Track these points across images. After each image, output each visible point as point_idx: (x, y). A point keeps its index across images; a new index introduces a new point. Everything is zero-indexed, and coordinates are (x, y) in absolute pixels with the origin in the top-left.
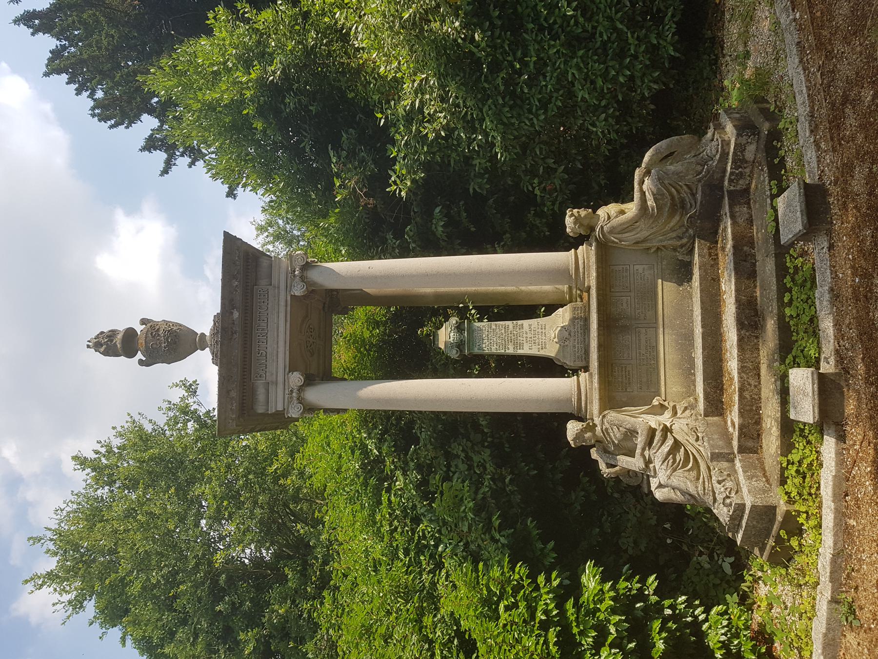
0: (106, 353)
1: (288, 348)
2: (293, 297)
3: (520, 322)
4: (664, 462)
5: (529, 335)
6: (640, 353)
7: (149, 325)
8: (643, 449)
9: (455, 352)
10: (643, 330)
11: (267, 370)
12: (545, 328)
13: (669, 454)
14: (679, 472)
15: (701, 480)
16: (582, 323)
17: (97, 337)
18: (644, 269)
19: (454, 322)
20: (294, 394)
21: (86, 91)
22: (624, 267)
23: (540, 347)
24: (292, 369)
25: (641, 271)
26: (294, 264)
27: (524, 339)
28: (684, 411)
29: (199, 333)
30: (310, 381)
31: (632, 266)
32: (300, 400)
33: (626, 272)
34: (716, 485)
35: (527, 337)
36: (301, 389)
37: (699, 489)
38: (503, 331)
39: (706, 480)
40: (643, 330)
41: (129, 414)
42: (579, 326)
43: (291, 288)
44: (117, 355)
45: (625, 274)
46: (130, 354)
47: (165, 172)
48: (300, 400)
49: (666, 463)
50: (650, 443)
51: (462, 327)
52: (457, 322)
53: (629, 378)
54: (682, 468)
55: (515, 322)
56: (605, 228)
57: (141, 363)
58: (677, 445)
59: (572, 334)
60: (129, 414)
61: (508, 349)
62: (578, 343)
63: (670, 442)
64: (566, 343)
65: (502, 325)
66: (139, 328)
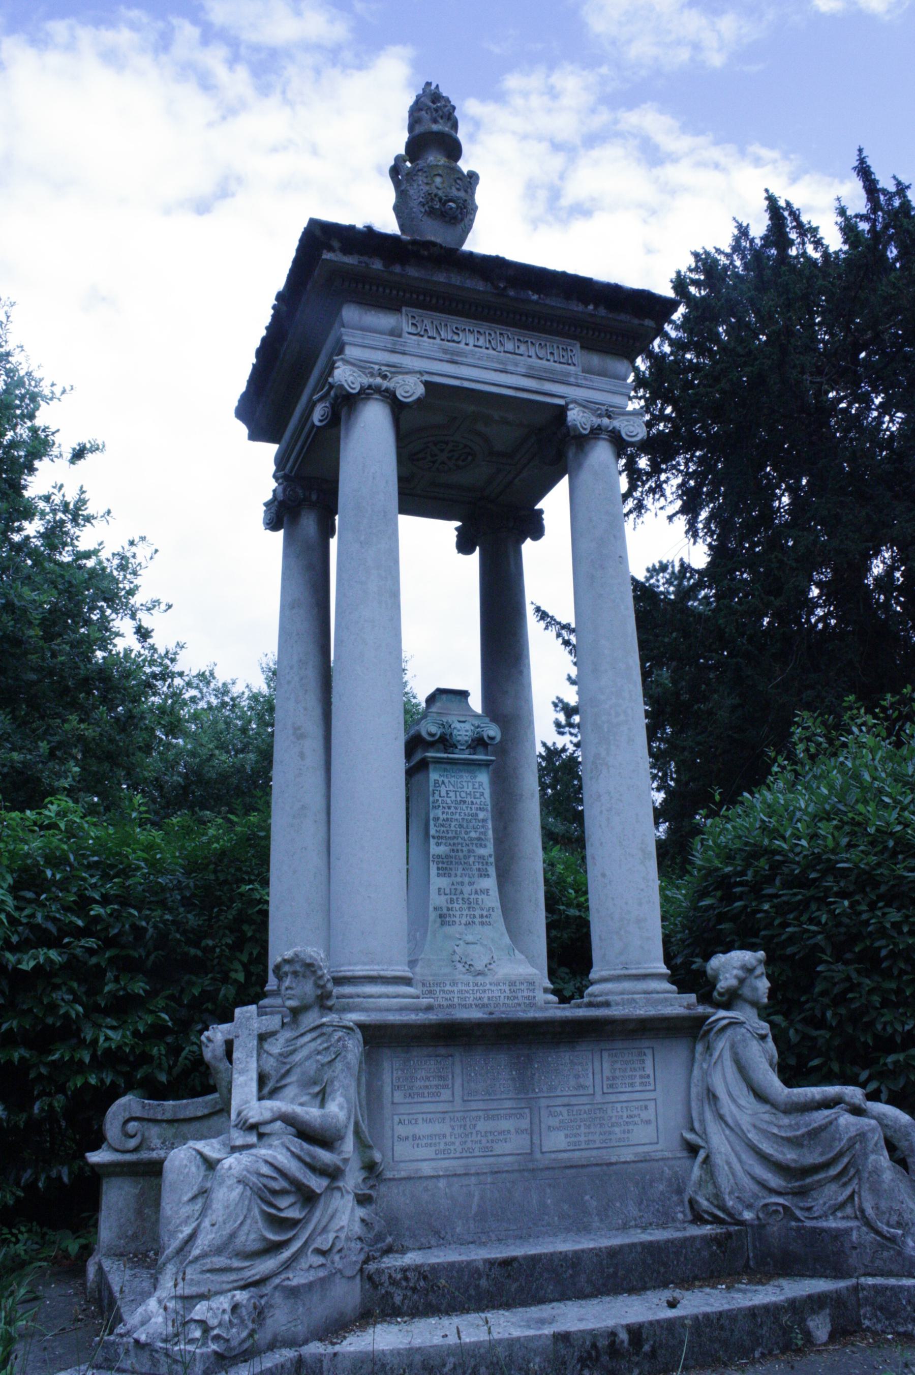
1: (466, 384)
3: (492, 871)
5: (467, 889)
6: (478, 1118)
8: (288, 1120)
9: (433, 729)
10: (525, 1124)
11: (425, 339)
12: (482, 924)
15: (236, 1263)
16: (502, 1001)
19: (492, 733)
20: (379, 380)
21: (765, 238)
22: (651, 1080)
23: (445, 911)
24: (427, 384)
25: (644, 1115)
26: (622, 418)
27: (459, 879)
31: (652, 1095)
33: (641, 1084)
35: (462, 883)
37: (215, 1259)
38: (473, 835)
39: (233, 1277)
40: (525, 1124)
41: (58, 431)
42: (497, 994)
44: (411, 128)
45: (638, 1080)
51: (480, 749)
52: (492, 738)
53: (423, 1095)
54: (263, 1212)
55: (492, 860)
59: (480, 979)
60: (58, 431)
61: (438, 844)
62: (460, 992)
63: (317, 1184)
64: (459, 966)
65: (485, 833)
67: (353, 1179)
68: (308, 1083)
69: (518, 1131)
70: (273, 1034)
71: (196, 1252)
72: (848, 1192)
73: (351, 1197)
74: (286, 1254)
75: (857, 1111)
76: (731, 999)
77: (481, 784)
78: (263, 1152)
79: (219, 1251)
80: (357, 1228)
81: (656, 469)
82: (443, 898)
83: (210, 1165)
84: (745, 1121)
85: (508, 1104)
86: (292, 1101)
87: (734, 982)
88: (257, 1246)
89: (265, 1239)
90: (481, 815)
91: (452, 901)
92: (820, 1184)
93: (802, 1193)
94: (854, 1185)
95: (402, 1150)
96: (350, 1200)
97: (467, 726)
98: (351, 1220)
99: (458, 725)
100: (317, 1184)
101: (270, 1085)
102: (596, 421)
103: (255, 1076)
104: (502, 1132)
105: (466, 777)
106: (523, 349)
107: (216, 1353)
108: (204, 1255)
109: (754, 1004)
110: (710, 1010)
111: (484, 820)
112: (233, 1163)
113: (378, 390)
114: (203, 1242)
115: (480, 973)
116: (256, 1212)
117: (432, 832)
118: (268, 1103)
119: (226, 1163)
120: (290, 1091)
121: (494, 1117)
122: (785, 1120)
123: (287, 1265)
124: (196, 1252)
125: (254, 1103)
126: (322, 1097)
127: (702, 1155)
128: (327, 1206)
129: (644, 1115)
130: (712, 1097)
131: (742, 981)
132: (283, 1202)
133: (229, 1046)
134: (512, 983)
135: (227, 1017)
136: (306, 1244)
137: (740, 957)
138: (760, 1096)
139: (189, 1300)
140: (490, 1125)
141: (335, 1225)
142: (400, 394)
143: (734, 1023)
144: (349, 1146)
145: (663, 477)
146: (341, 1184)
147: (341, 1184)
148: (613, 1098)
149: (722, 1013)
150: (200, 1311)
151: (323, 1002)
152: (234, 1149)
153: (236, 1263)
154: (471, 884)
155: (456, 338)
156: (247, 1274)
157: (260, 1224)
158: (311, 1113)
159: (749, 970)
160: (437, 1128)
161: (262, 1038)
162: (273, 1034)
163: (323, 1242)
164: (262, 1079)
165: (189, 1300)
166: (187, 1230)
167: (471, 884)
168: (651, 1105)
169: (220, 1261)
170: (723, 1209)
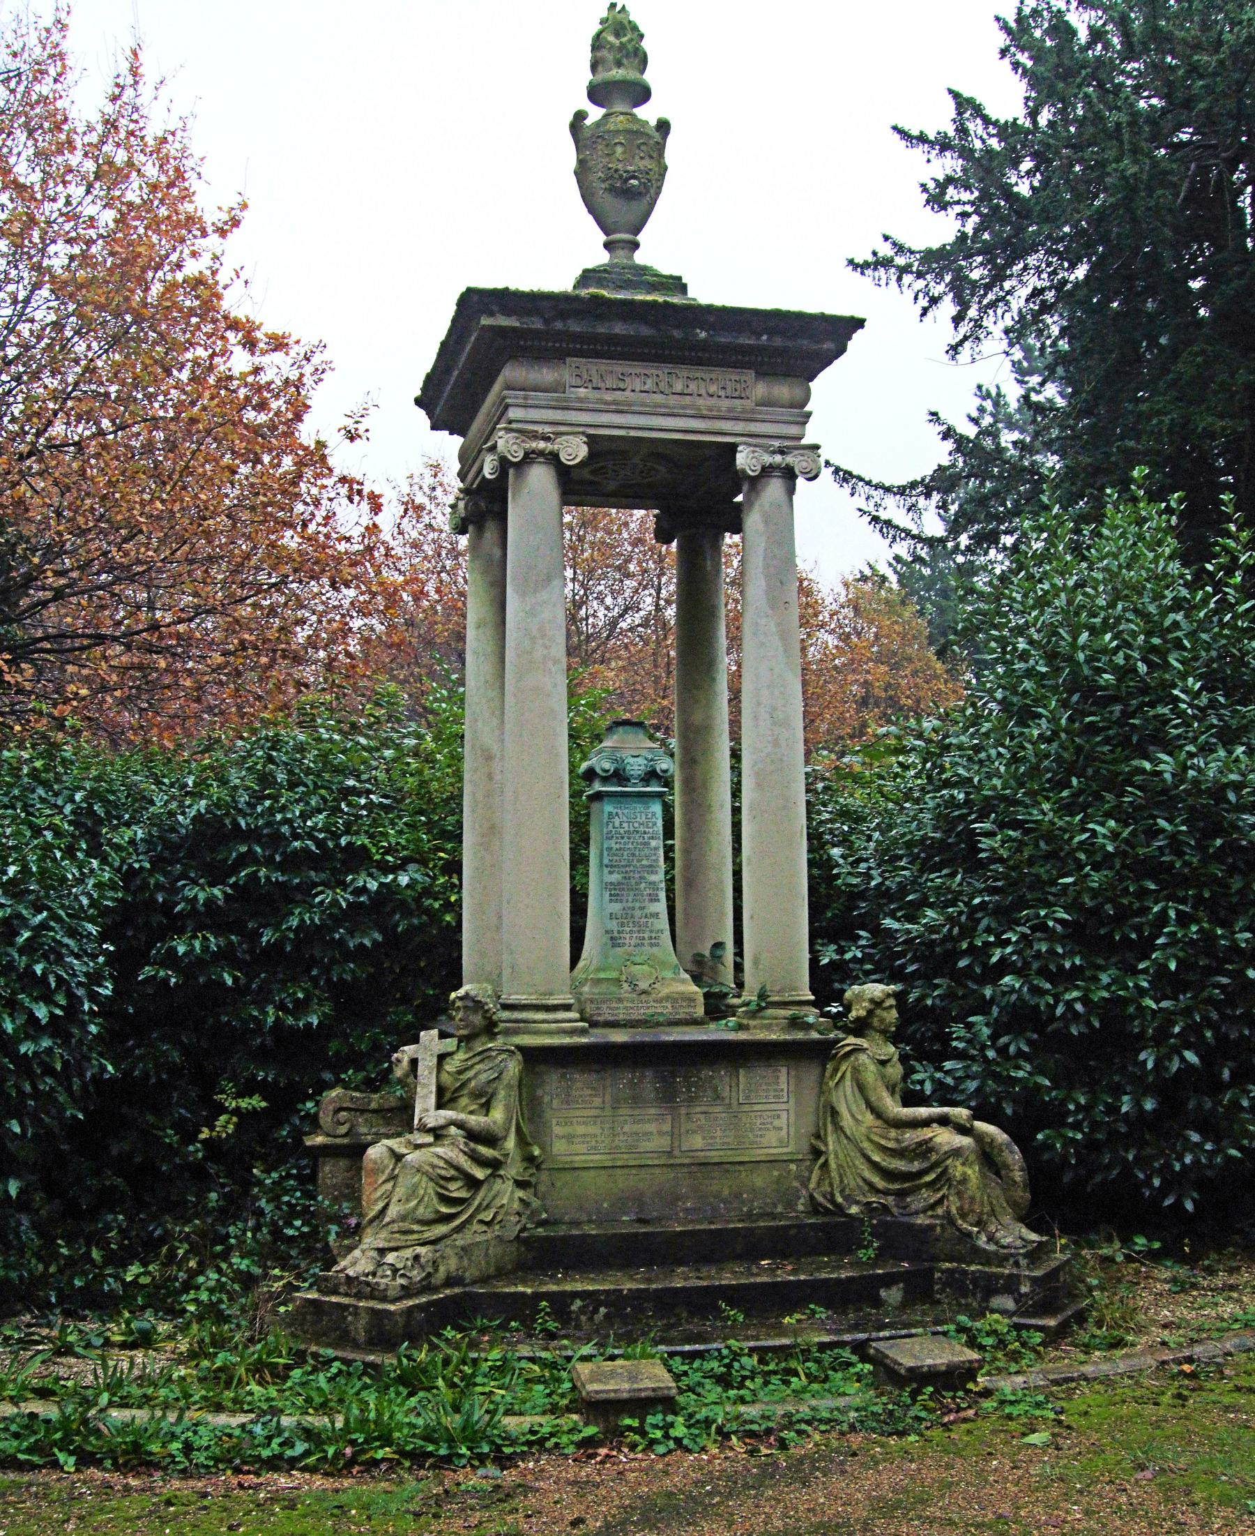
0: (597, 44)
1: (633, 433)
2: (733, 448)
4: (446, 1161)
5: (638, 913)
7: (657, 135)
8: (460, 1125)
9: (607, 766)
12: (652, 945)
13: (457, 1168)
14: (431, 1188)
15: (416, 1227)
17: (635, 28)
18: (780, 1129)
24: (592, 441)
25: (777, 1123)
28: (521, 1200)
29: (640, 238)
30: (565, 475)
31: (784, 1106)
32: (529, 458)
34: (408, 1253)
36: (553, 458)
39: (415, 1236)
40: (667, 1127)
43: (750, 445)
46: (595, 94)
47: (903, 134)
48: (529, 458)
49: (442, 1164)
50: (473, 1136)
51: (654, 782)
56: (863, 1058)
57: (580, 116)
58: (473, 1184)
63: (480, 1174)
64: (625, 986)
66: (648, 113)
67: (513, 1169)
68: (475, 1095)
69: (661, 1133)
70: (450, 1054)
71: (387, 1219)
72: (939, 1195)
73: (511, 1183)
74: (457, 1222)
75: (963, 1130)
76: (861, 1028)
77: (654, 814)
78: (439, 1150)
79: (403, 1218)
80: (516, 1206)
81: (998, 277)
82: (615, 922)
83: (398, 1157)
84: (859, 1132)
85: (653, 1111)
86: (462, 1111)
87: (863, 1013)
88: (432, 1216)
89: (438, 1212)
90: (653, 843)
91: (622, 925)
92: (919, 1188)
93: (901, 1194)
94: (944, 1191)
95: (559, 1147)
96: (509, 1185)
97: (641, 761)
98: (511, 1199)
99: (631, 760)
100: (480, 1174)
101: (448, 1095)
102: (768, 459)
103: (434, 1089)
104: (646, 1134)
105: (639, 807)
106: (693, 387)
107: (402, 1286)
108: (393, 1222)
109: (883, 1032)
110: (841, 1035)
111: (656, 849)
112: (413, 1157)
113: (541, 453)
114: (393, 1212)
115: (644, 992)
116: (430, 1191)
117: (606, 861)
118: (442, 1112)
119: (409, 1158)
120: (464, 1101)
121: (639, 1122)
122: (893, 1133)
123: (458, 1229)
124: (387, 1219)
125: (432, 1112)
126: (486, 1107)
127: (822, 1160)
128: (490, 1190)
129: (777, 1123)
130: (835, 1113)
131: (870, 1013)
132: (453, 1186)
133: (414, 1062)
134: (675, 1000)
135: (416, 1040)
136: (472, 1216)
137: (876, 989)
138: (878, 1113)
139: (382, 1252)
140: (636, 1128)
141: (498, 1203)
142: (563, 458)
143: (858, 1050)
144: (511, 1143)
145: (1007, 285)
146: (502, 1172)
147: (502, 1172)
148: (746, 1108)
149: (851, 1040)
150: (391, 1258)
151: (490, 1028)
152: (418, 1147)
153: (416, 1227)
154: (642, 908)
155: (622, 385)
156: (426, 1235)
157: (435, 1201)
158: (475, 1121)
159: (877, 1003)
160: (592, 1129)
161: (442, 1058)
162: (450, 1054)
163: (487, 1216)
164: (441, 1090)
165: (382, 1252)
166: (381, 1205)
167: (642, 908)
168: (784, 1115)
169: (405, 1226)
170: (833, 1201)
